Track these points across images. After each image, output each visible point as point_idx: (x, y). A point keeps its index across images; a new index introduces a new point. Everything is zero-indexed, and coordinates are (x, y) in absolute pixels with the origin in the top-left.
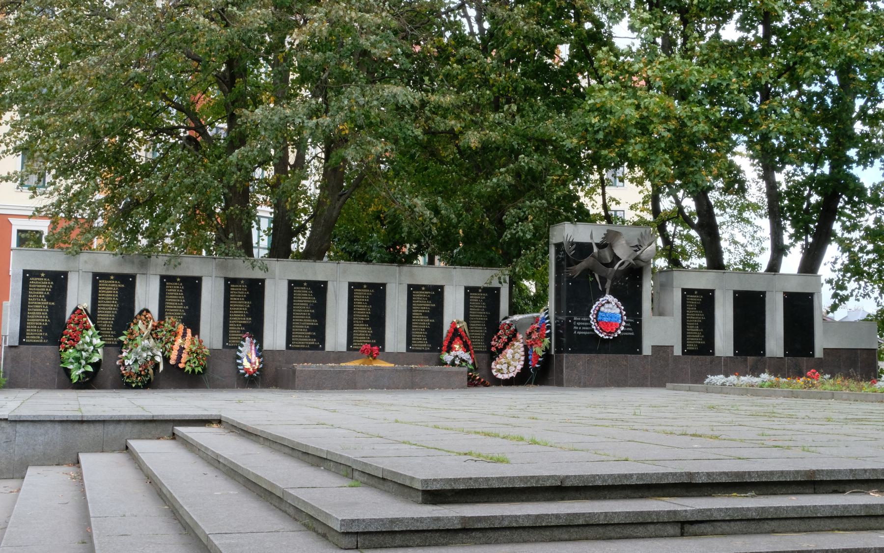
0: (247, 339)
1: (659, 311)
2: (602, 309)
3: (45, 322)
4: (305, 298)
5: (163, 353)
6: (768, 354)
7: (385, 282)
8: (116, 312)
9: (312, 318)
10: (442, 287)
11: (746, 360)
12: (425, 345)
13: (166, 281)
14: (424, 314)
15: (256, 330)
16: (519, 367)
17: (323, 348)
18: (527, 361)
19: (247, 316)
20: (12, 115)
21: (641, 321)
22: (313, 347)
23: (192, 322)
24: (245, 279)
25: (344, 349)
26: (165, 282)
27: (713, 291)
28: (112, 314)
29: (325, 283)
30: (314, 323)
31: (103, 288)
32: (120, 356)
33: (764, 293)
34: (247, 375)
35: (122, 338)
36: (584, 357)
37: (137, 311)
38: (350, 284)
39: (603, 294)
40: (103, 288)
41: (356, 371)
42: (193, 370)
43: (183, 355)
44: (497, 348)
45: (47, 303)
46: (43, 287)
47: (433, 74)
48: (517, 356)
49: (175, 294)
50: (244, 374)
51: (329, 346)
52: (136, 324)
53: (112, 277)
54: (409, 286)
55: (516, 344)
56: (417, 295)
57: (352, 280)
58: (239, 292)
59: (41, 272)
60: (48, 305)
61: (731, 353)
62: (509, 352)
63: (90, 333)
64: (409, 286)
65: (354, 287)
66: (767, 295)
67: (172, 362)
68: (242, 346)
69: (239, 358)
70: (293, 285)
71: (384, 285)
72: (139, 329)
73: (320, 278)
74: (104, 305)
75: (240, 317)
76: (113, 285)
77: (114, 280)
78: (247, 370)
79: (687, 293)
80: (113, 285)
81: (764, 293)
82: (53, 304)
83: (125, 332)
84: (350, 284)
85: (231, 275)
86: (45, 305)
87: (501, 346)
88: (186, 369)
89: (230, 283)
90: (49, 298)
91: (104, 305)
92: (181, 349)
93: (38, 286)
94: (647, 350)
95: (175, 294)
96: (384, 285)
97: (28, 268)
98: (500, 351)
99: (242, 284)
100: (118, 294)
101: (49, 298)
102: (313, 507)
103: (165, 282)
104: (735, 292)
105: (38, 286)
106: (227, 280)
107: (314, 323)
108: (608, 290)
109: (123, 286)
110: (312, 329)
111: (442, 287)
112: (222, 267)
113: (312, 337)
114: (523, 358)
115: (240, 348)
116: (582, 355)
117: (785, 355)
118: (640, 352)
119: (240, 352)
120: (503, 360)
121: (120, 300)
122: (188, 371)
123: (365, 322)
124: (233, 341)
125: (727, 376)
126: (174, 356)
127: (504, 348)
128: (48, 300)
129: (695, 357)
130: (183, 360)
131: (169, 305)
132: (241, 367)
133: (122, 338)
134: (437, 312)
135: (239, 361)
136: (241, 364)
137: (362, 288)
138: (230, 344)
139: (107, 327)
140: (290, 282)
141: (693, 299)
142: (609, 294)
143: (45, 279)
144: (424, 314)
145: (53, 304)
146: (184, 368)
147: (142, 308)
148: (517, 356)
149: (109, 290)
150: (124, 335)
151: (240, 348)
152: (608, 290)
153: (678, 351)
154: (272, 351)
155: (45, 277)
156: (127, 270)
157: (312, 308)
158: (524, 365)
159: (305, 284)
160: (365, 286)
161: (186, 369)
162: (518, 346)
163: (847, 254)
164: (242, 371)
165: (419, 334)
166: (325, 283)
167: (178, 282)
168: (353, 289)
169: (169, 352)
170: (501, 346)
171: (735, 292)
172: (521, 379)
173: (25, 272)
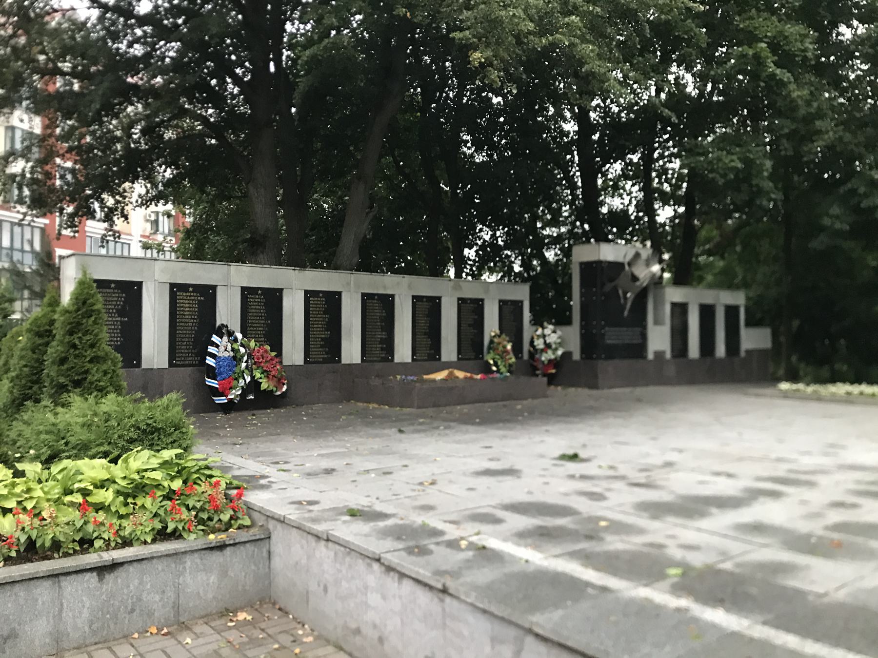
1: (657, 322)
3: (117, 341)
4: (378, 312)
7: (140, 280)
8: (196, 328)
10: (482, 300)
14: (470, 325)
19: (326, 330)
20: (88, 14)
22: (385, 360)
28: (192, 330)
30: (384, 335)
31: (182, 301)
40: (182, 301)
45: (119, 319)
49: (257, 307)
53: (321, 295)
60: (121, 322)
65: (247, 293)
71: (439, 298)
74: (183, 320)
76: (192, 298)
77: (427, 301)
79: (674, 305)
80: (192, 298)
82: (126, 319)
86: (117, 321)
91: (183, 320)
95: (257, 307)
96: (439, 298)
99: (320, 297)
100: (198, 308)
101: (121, 313)
102: (466, 442)
107: (384, 335)
109: (203, 298)
110: (382, 341)
113: (382, 349)
123: (425, 334)
134: (479, 324)
139: (187, 345)
140: (306, 292)
141: (425, 305)
143: (116, 291)
144: (470, 325)
145: (126, 319)
153: (668, 355)
154: (349, 365)
155: (262, 294)
160: (191, 289)
167: (259, 295)
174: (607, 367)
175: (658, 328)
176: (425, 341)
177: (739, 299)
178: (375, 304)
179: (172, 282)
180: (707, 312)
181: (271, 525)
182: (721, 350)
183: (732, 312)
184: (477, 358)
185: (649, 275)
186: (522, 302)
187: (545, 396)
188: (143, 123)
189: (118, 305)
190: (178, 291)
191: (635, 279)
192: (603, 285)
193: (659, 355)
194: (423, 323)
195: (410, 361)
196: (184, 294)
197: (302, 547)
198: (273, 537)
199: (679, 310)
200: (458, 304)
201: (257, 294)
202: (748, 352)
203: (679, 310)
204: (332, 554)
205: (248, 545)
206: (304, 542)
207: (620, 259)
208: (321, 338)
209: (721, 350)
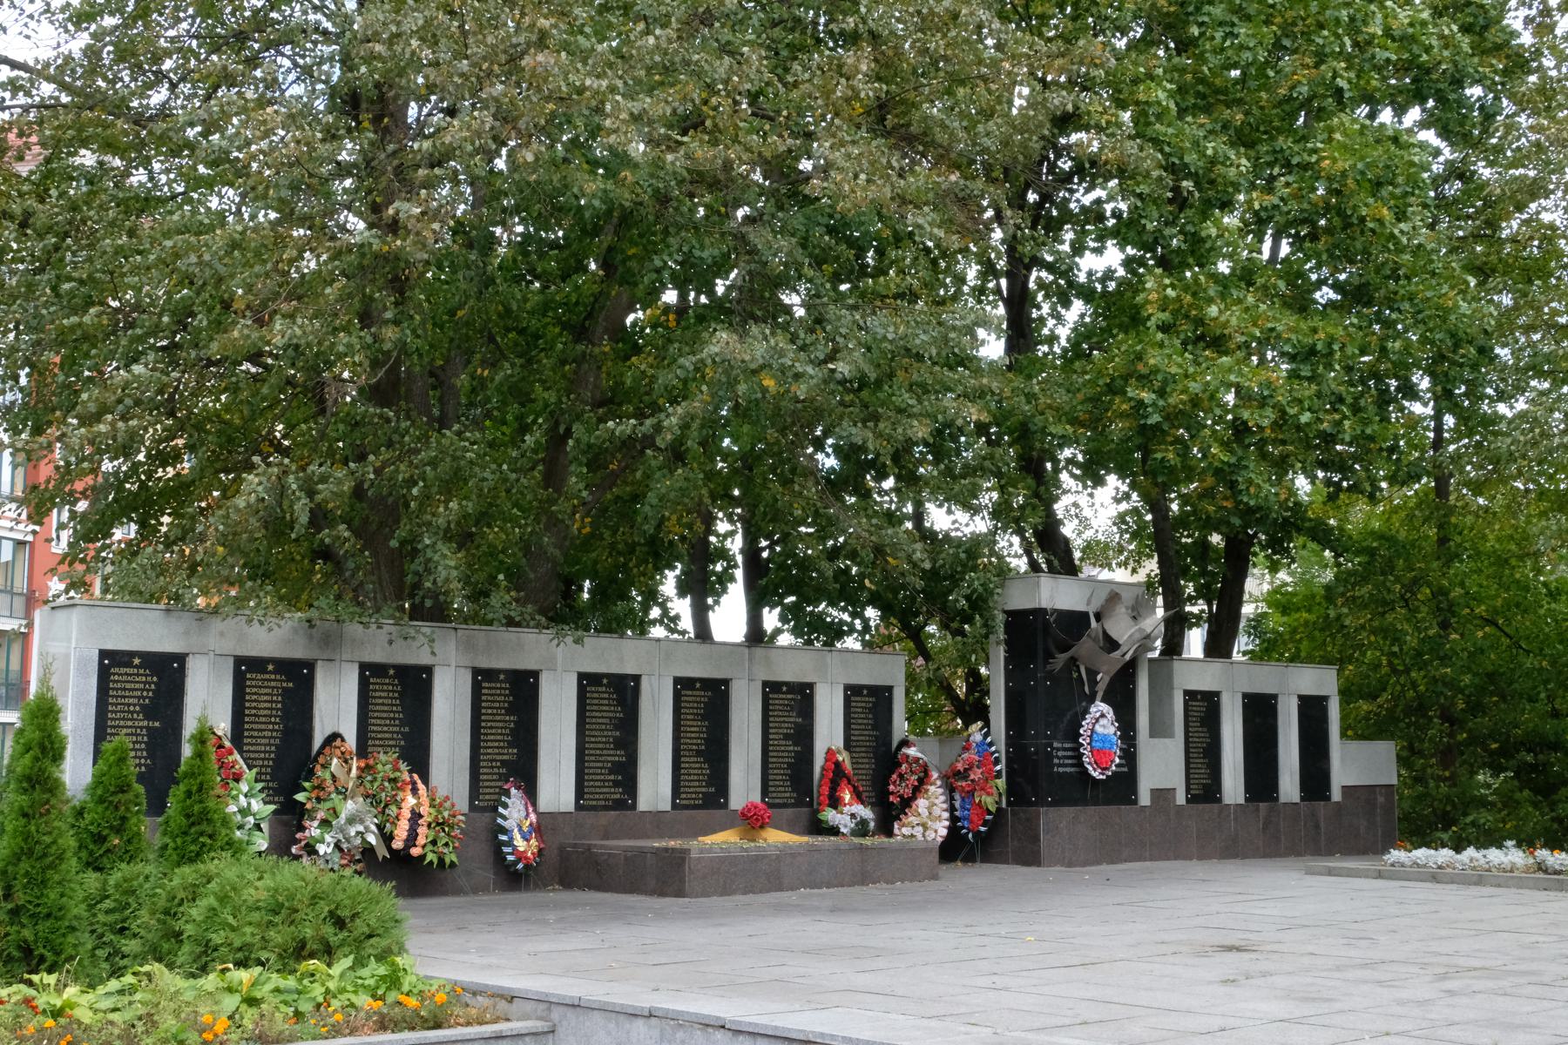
0: (513, 791)
2: (1098, 728)
4: (605, 710)
5: (380, 827)
6: (1283, 799)
9: (615, 749)
10: (811, 686)
11: (1257, 810)
12: (788, 795)
13: (370, 673)
15: (525, 774)
16: (944, 832)
17: (634, 806)
18: (954, 819)
21: (1134, 746)
22: (620, 805)
23: (418, 757)
24: (506, 672)
25: (667, 806)
26: (245, 673)
27: (1217, 694)
29: (637, 678)
30: (619, 756)
32: (298, 836)
33: (1275, 697)
34: (520, 866)
35: (300, 797)
36: (1068, 812)
37: (317, 742)
38: (677, 681)
39: (1092, 700)
41: (786, 853)
42: (441, 861)
43: (420, 830)
44: (901, 797)
46: (136, 687)
47: (716, 218)
48: (937, 811)
50: (515, 863)
51: (644, 803)
52: (325, 766)
53: (270, 667)
54: (765, 684)
55: (932, 789)
56: (778, 699)
57: (679, 674)
58: (498, 694)
59: (132, 654)
60: (148, 728)
61: (1241, 800)
62: (921, 804)
63: (244, 787)
64: (765, 684)
65: (587, 681)
66: (1280, 699)
67: (398, 844)
68: (505, 806)
69: (504, 831)
70: (587, 681)
71: (726, 682)
72: (333, 776)
73: (629, 669)
75: (500, 750)
77: (274, 672)
78: (520, 856)
79: (1190, 695)
81: (1275, 697)
82: (157, 724)
83: (307, 785)
84: (677, 681)
85: (485, 663)
87: (908, 792)
88: (428, 859)
89: (482, 677)
90: (149, 712)
92: (416, 816)
93: (128, 686)
94: (1145, 799)
96: (726, 682)
97: (110, 646)
98: (907, 803)
101: (149, 712)
103: (245, 673)
104: (1245, 696)
105: (128, 686)
106: (476, 672)
107: (619, 756)
108: (1100, 695)
110: (616, 768)
111: (811, 686)
112: (468, 646)
113: (616, 784)
114: (946, 815)
115: (501, 810)
116: (1065, 809)
117: (1302, 799)
118: (1135, 802)
119: (505, 818)
120: (912, 819)
121: (286, 716)
122: (431, 862)
123: (699, 753)
124: (486, 798)
125: (1458, 849)
126: (401, 832)
127: (914, 798)
128: (147, 718)
129: (1201, 806)
130: (421, 840)
131: (375, 725)
132: (509, 850)
133: (300, 797)
134: (804, 735)
135: (504, 838)
136: (510, 843)
137: (694, 689)
138: (485, 801)
140: (582, 676)
141: (703, 696)
142: (1103, 701)
144: (787, 737)
145: (157, 724)
146: (423, 857)
147: (328, 732)
148: (937, 811)
149: (267, 694)
150: (305, 790)
151: (501, 810)
152: (1100, 695)
153: (1181, 799)
156: (298, 652)
157: (616, 728)
158: (949, 828)
159: (137, 661)
160: (137, 661)
161: (428, 859)
162: (936, 791)
163: (778, 609)
164: (511, 858)
165: (779, 775)
166: (637, 678)
168: (109, 667)
169: (393, 823)
170: (908, 792)
171: (1245, 696)
172: (955, 849)
173: (104, 654)
174: (1056, 822)
175: (1159, 742)
176: (697, 769)
177: (1320, 680)
178: (600, 694)
179: (239, 653)
180: (1260, 710)
181: (556, 1014)
182: (1289, 785)
183: (1312, 709)
184: (799, 803)
185: (1138, 636)
186: (890, 689)
187: (935, 877)
188: (838, 645)
189: (144, 698)
190: (372, 676)
191: (1112, 645)
192: (1049, 655)
193: (1161, 795)
194: (696, 732)
195: (668, 808)
196: (259, 676)
197: (609, 1033)
198: (560, 1030)
199: (1204, 708)
200: (101, 663)
201: (601, 685)
202: (1346, 790)
203: (1204, 708)
204: (656, 1033)
205: (527, 1039)
206: (612, 1026)
207: (1080, 607)
208: (502, 762)
209: (1289, 785)
